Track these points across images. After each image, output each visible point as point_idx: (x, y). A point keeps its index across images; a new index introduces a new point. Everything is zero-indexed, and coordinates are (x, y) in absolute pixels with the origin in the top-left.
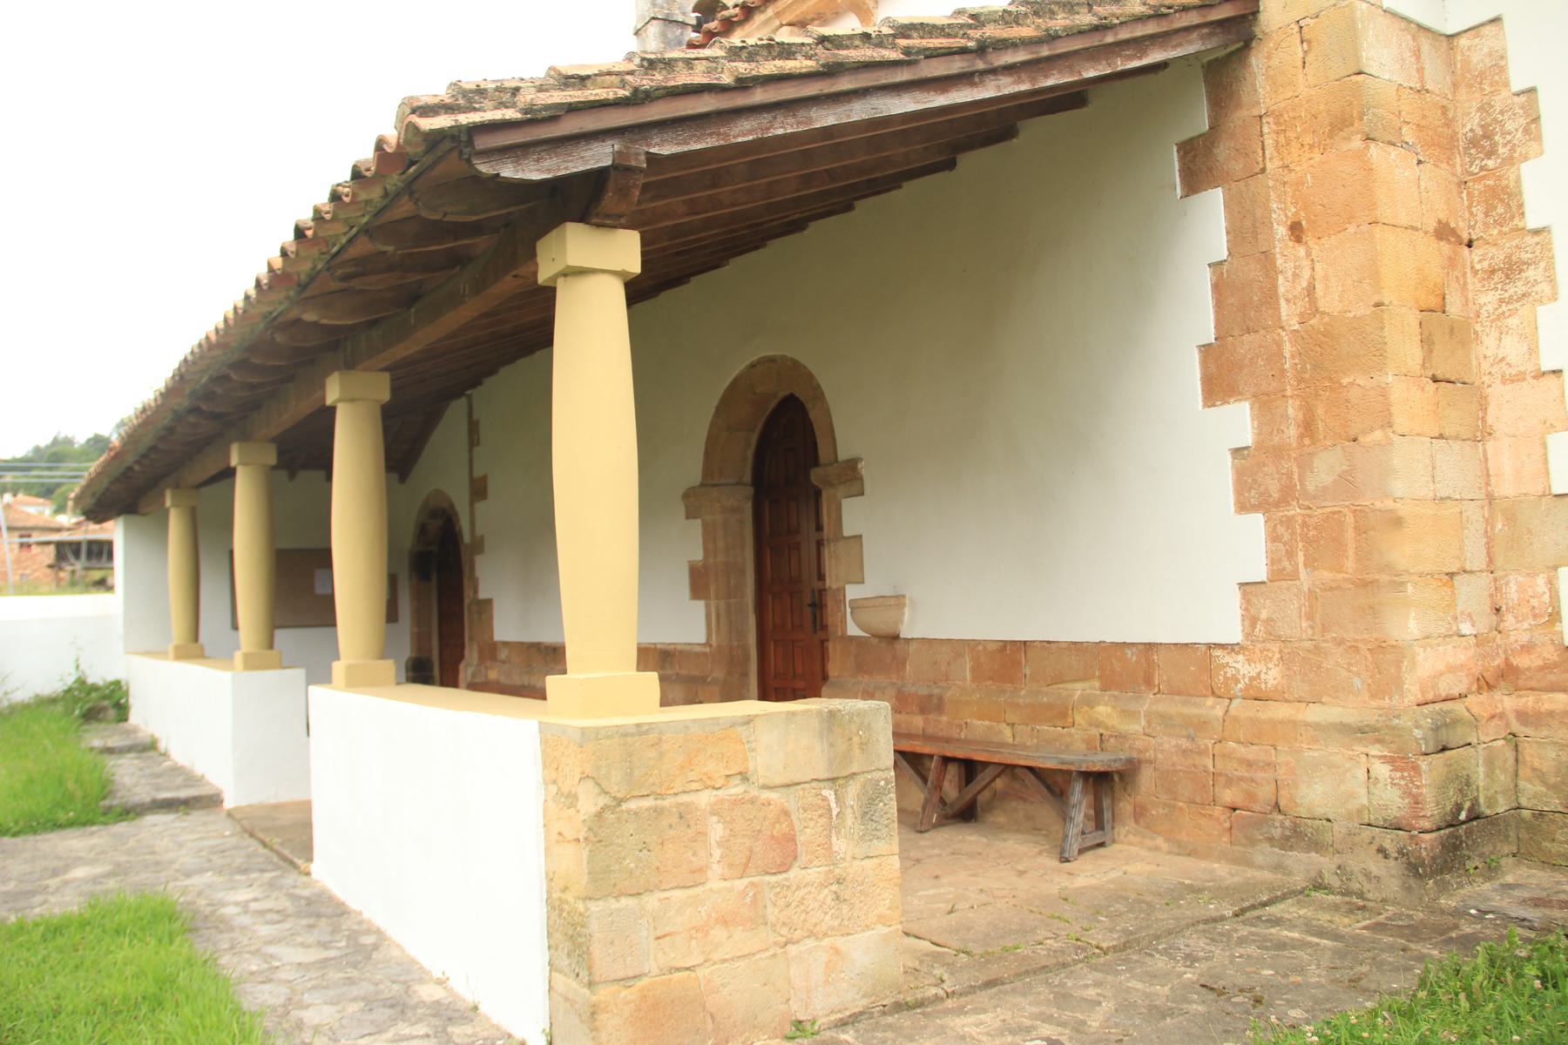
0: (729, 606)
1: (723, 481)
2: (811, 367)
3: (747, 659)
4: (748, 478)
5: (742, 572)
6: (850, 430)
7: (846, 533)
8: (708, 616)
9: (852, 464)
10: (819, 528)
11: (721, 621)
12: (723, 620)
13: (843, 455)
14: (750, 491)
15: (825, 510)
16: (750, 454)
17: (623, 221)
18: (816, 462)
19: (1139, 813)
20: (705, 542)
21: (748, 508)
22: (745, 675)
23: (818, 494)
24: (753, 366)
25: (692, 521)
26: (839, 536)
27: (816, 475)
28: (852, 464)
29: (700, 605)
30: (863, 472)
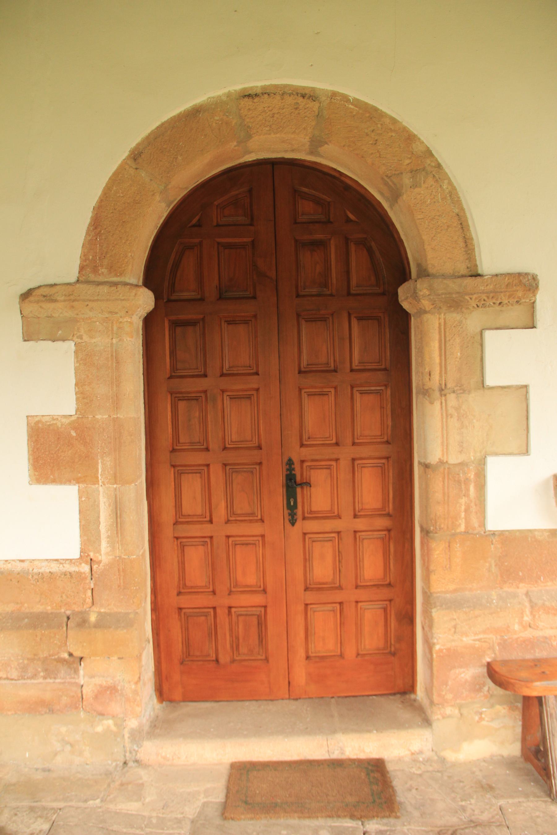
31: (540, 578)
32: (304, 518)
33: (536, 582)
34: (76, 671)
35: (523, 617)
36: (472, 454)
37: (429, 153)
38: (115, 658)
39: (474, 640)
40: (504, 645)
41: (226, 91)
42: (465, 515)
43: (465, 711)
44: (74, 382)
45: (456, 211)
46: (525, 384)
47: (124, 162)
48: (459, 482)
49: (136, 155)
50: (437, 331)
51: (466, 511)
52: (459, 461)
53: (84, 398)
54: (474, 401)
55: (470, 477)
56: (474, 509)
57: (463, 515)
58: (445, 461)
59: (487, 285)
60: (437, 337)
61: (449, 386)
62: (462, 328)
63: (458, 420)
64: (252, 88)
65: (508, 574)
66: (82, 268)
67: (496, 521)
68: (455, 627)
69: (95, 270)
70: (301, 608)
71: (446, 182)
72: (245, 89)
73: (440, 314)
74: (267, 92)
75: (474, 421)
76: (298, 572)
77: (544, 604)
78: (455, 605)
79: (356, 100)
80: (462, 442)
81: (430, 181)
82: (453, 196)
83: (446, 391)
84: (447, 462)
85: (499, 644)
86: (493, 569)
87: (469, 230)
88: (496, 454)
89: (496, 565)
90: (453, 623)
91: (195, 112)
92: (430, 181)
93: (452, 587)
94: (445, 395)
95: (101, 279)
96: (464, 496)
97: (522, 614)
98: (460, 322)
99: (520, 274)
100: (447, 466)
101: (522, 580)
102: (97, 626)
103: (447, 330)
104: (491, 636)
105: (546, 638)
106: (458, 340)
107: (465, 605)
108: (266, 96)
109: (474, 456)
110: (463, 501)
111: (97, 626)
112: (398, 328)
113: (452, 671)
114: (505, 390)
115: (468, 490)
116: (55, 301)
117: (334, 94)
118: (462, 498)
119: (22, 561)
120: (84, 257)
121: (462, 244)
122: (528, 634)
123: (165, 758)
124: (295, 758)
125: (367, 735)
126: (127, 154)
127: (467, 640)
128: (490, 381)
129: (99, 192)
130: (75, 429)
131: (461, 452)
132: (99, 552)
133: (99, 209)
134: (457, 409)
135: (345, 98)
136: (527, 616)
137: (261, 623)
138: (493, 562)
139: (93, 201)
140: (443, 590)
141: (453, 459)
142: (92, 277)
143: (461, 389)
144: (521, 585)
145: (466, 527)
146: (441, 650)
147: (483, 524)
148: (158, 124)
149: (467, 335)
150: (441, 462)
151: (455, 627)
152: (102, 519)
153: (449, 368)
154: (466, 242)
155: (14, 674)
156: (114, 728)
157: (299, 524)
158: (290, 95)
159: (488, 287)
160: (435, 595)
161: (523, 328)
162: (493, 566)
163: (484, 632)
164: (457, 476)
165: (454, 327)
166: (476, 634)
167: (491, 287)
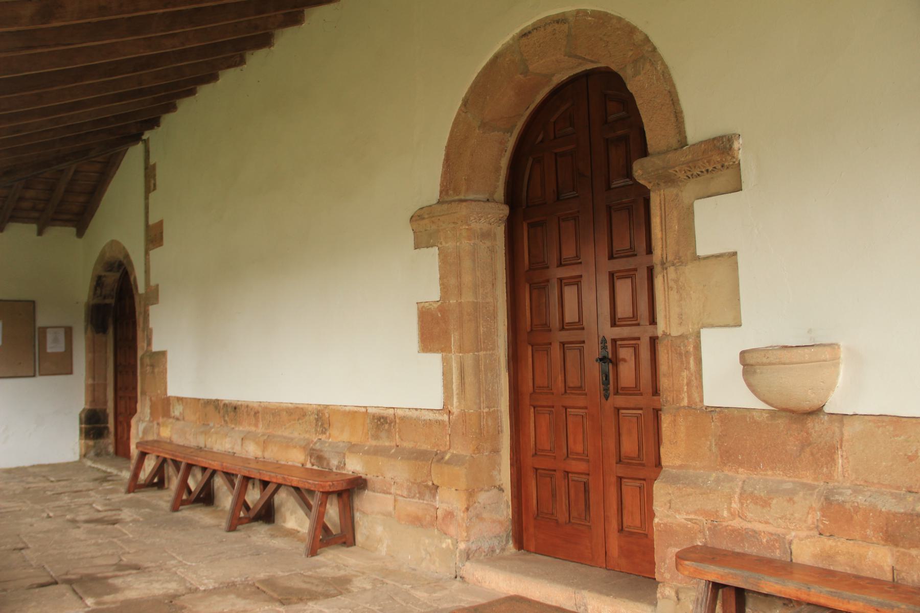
1: (471, 197)
3: (500, 432)
4: (500, 194)
5: (494, 316)
12: (470, 379)
13: (697, 130)
14: (505, 211)
15: (656, 221)
16: (504, 162)
21: (500, 232)
22: (496, 451)
24: (525, 34)
30: (741, 156)
32: (617, 393)
33: (756, 468)
34: (434, 496)
35: (731, 503)
37: (647, 40)
38: (453, 489)
39: (686, 519)
40: (714, 530)
41: (511, 36)
43: (682, 596)
44: (438, 276)
45: (668, 88)
46: (731, 250)
47: (460, 109)
48: (680, 354)
49: (465, 103)
50: (658, 208)
51: (688, 384)
52: (679, 334)
53: (444, 288)
54: (690, 272)
56: (695, 383)
57: (685, 388)
60: (659, 214)
64: (526, 28)
65: (728, 456)
66: (441, 192)
67: (710, 400)
68: (670, 502)
69: (447, 193)
70: (613, 479)
71: (659, 63)
72: (522, 30)
73: (659, 190)
74: (536, 27)
76: (611, 445)
77: (752, 493)
78: (674, 480)
79: (593, 11)
81: (648, 66)
82: (666, 76)
83: (667, 265)
85: (709, 529)
86: (714, 449)
87: (679, 104)
88: (712, 326)
90: (668, 498)
91: (496, 57)
92: (648, 66)
93: (678, 463)
95: (450, 198)
97: (730, 499)
98: (677, 195)
99: (714, 139)
100: (670, 338)
101: (741, 464)
102: (447, 463)
104: (701, 518)
105: (755, 532)
106: (675, 213)
110: (685, 374)
111: (447, 463)
112: (637, 206)
113: (669, 549)
115: (688, 363)
116: (424, 219)
117: (578, 12)
119: (416, 409)
120: (442, 185)
121: (673, 119)
122: (737, 523)
123: (477, 579)
124: (554, 604)
125: (604, 598)
126: (460, 103)
127: (681, 518)
128: (701, 251)
129: (447, 135)
130: (440, 311)
131: (681, 324)
132: (452, 405)
133: (448, 148)
134: (676, 281)
135: (585, 12)
137: (586, 491)
139: (445, 143)
141: (674, 333)
142: (447, 199)
143: (679, 261)
144: (741, 470)
146: (659, 524)
147: (702, 401)
148: (476, 75)
150: (665, 334)
151: (670, 502)
152: (454, 380)
153: (668, 242)
154: (676, 117)
155: (405, 493)
156: (451, 546)
158: (549, 24)
163: (695, 513)
166: (687, 513)
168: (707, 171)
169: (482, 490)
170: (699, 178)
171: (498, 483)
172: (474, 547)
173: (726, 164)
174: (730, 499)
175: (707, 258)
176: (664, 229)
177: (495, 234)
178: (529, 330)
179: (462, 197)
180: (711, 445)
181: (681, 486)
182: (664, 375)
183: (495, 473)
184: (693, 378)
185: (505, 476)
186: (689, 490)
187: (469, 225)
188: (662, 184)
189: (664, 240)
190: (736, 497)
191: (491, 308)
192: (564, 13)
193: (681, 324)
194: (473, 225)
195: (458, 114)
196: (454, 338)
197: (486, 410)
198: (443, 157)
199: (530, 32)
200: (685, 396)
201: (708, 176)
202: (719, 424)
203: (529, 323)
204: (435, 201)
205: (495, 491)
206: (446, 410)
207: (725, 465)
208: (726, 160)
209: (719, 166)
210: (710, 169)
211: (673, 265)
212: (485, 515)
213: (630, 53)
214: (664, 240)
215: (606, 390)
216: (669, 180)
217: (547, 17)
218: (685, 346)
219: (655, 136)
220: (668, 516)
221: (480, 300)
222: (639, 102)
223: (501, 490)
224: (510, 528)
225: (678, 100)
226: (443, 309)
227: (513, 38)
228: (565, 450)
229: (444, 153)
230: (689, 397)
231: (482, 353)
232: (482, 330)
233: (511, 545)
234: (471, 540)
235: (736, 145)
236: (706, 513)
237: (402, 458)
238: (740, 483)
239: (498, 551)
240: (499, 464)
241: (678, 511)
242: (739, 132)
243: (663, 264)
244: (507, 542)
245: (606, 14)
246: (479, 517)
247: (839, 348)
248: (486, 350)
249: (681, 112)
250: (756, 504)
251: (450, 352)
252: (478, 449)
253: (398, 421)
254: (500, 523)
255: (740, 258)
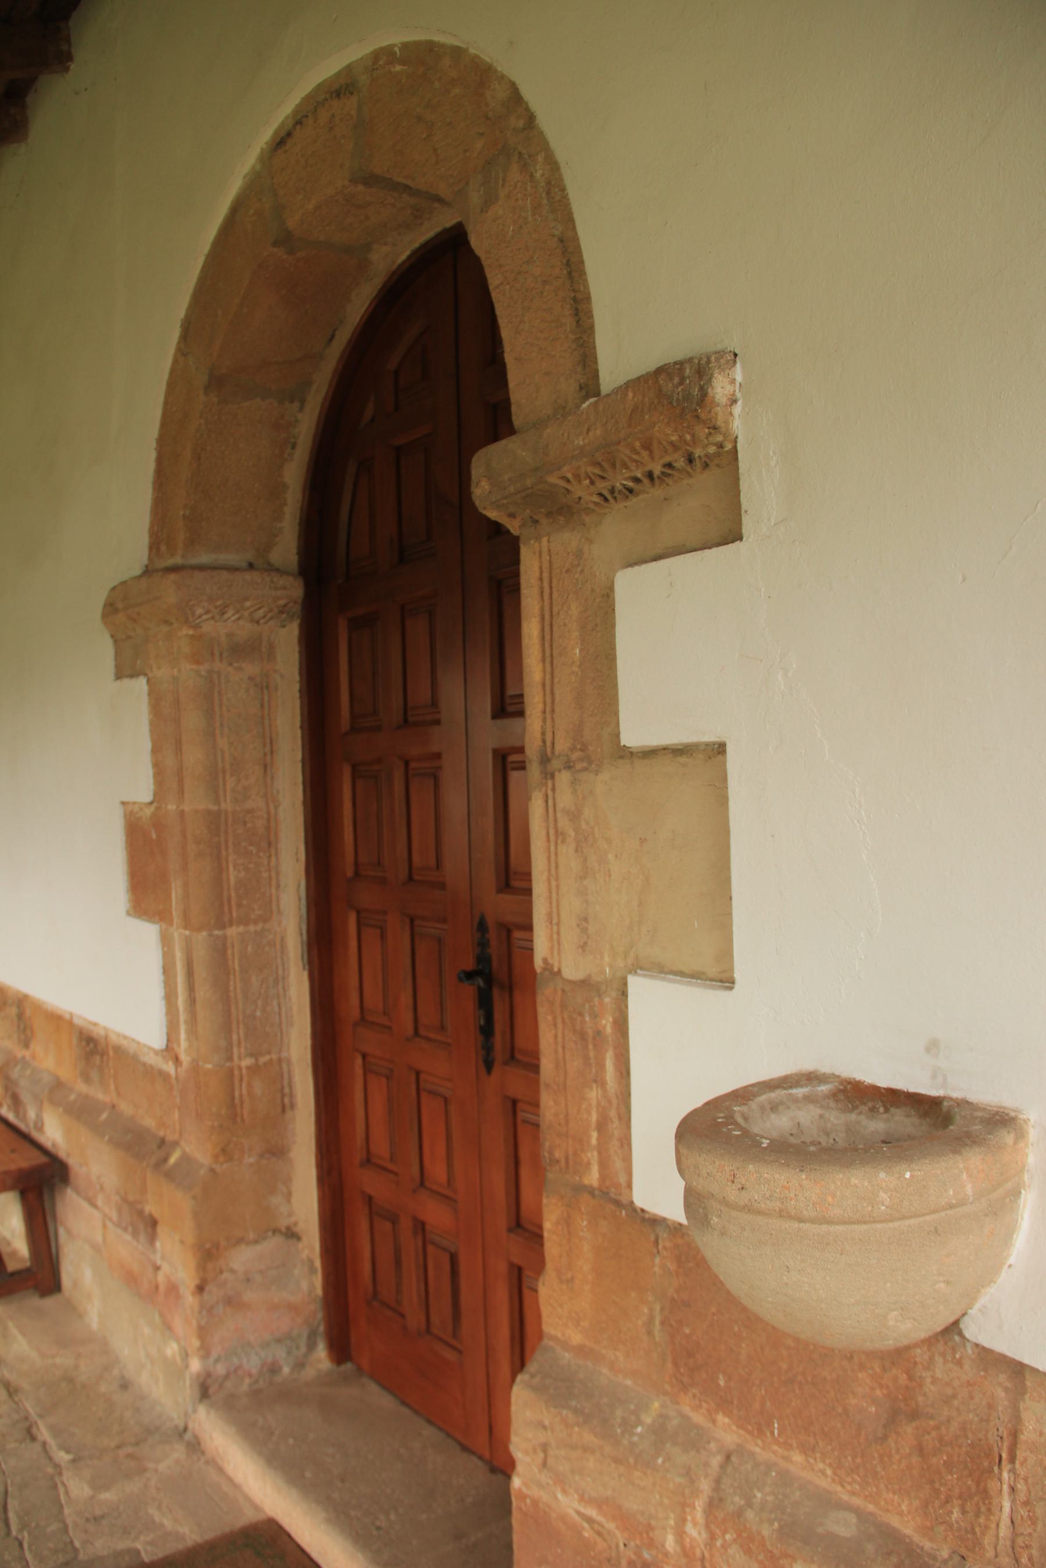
0: (220, 950)
1: (205, 558)
2: (486, 44)
3: (285, 1105)
4: (287, 548)
5: (269, 842)
6: (652, 252)
7: (634, 733)
8: (168, 970)
9: (681, 391)
10: (507, 706)
11: (214, 983)
12: (203, 992)
13: (624, 352)
14: (296, 589)
15: (531, 630)
16: (294, 474)
17: (623, 1007)
18: (498, 422)
19: (295, 602)
20: (155, 750)
21: (287, 640)
22: (277, 1151)
23: (501, 549)
24: (281, 142)
25: (126, 682)
26: (598, 745)
27: (494, 479)
28: (681, 391)
29: (148, 932)
30: (738, 423)
31: (770, 1424)
36: (606, 959)
37: (516, 98)
38: (177, 1237)
42: (598, 1139)
46: (710, 737)
47: (178, 350)
48: (583, 1036)
50: (536, 591)
51: (601, 1127)
55: (604, 1027)
58: (556, 969)
59: (588, 430)
61: (558, 748)
62: (582, 571)
63: (576, 851)
71: (540, 158)
72: (276, 132)
73: (538, 539)
74: (299, 120)
75: (610, 856)
79: (405, 46)
80: (586, 919)
81: (515, 174)
83: (556, 764)
84: (559, 970)
89: (662, 1323)
92: (515, 174)
93: (576, 1338)
94: (553, 777)
96: (595, 1081)
97: (684, 1505)
98: (579, 554)
103: (555, 582)
107: (574, 1403)
108: (298, 127)
109: (611, 967)
110: (593, 1094)
114: (683, 759)
115: (601, 1066)
117: (377, 55)
118: (591, 1089)
121: (569, 322)
134: (575, 816)
136: (695, 1524)
138: (657, 1307)
140: (559, 1335)
144: (722, 1419)
145: (603, 1177)
149: (593, 590)
154: (576, 313)
157: (497, 1069)
159: (591, 434)
160: (546, 1342)
161: (719, 544)
162: (657, 1322)
164: (579, 1019)
165: (567, 571)
167: (598, 432)
168: (650, 475)
169: (241, 1241)
170: (634, 500)
171: (283, 1223)
172: (221, 1369)
173: (698, 452)
174: (683, 1506)
175: (650, 753)
176: (549, 658)
177: (271, 647)
178: (350, 873)
179: (178, 560)
180: (651, 1318)
181: (571, 1418)
182: (547, 1086)
183: (276, 1200)
184: (613, 1113)
185: (303, 1201)
186: (589, 1438)
187: (197, 627)
188: (544, 521)
189: (549, 687)
190: (699, 1505)
191: (260, 824)
192: (349, 68)
193: (583, 947)
194: (208, 627)
195: (175, 361)
196: (176, 892)
197: (247, 1062)
198: (152, 466)
199: (289, 134)
200: (593, 1156)
201: (657, 492)
202: (672, 1266)
203: (350, 857)
204: (138, 571)
205: (278, 1239)
206: (170, 1051)
207: (684, 1388)
208: (695, 441)
209: (680, 463)
210: (657, 470)
211: (569, 766)
212: (250, 1296)
213: (479, 145)
214: (549, 687)
215: (488, 1049)
216: (558, 509)
217: (319, 86)
218: (595, 1016)
219: (531, 378)
220: (540, 1485)
221: (227, 805)
222: (494, 280)
223: (292, 1234)
224: (320, 1315)
225: (582, 262)
226: (158, 822)
227: (261, 159)
228: (415, 1170)
229: (153, 455)
230: (604, 1165)
231: (232, 932)
232: (233, 875)
233: (321, 1352)
234: (214, 1355)
235: (720, 388)
236: (624, 1518)
237: (110, 1141)
238: (716, 1461)
239: (286, 1370)
240: (288, 1180)
241: (560, 1480)
242: (734, 344)
243: (545, 760)
244: (311, 1346)
245: (430, 47)
246: (232, 1302)
247: (1021, 1135)
248: (245, 921)
249: (588, 299)
250: (748, 1552)
251: (171, 924)
252: (225, 1152)
253: (111, 1053)
254: (292, 1308)
255: (733, 760)
